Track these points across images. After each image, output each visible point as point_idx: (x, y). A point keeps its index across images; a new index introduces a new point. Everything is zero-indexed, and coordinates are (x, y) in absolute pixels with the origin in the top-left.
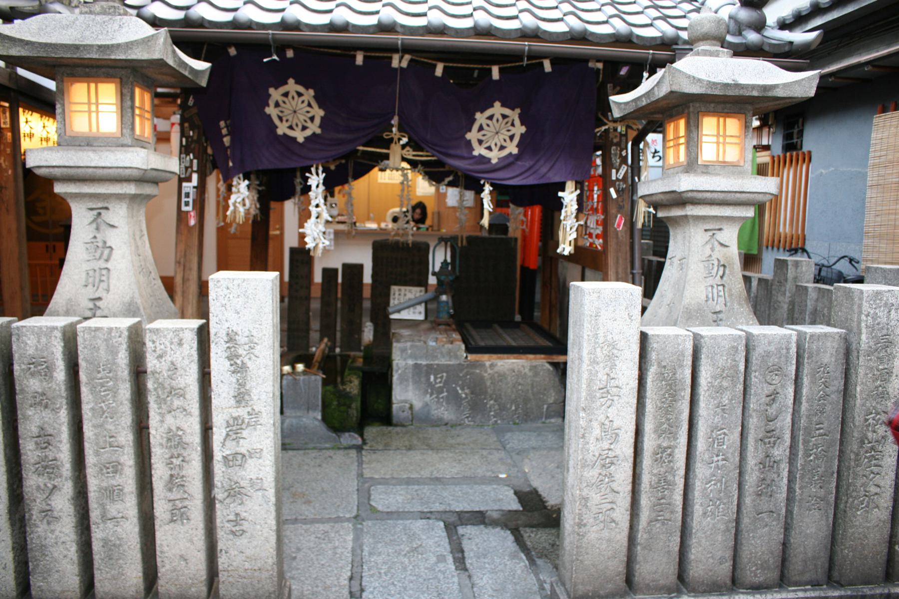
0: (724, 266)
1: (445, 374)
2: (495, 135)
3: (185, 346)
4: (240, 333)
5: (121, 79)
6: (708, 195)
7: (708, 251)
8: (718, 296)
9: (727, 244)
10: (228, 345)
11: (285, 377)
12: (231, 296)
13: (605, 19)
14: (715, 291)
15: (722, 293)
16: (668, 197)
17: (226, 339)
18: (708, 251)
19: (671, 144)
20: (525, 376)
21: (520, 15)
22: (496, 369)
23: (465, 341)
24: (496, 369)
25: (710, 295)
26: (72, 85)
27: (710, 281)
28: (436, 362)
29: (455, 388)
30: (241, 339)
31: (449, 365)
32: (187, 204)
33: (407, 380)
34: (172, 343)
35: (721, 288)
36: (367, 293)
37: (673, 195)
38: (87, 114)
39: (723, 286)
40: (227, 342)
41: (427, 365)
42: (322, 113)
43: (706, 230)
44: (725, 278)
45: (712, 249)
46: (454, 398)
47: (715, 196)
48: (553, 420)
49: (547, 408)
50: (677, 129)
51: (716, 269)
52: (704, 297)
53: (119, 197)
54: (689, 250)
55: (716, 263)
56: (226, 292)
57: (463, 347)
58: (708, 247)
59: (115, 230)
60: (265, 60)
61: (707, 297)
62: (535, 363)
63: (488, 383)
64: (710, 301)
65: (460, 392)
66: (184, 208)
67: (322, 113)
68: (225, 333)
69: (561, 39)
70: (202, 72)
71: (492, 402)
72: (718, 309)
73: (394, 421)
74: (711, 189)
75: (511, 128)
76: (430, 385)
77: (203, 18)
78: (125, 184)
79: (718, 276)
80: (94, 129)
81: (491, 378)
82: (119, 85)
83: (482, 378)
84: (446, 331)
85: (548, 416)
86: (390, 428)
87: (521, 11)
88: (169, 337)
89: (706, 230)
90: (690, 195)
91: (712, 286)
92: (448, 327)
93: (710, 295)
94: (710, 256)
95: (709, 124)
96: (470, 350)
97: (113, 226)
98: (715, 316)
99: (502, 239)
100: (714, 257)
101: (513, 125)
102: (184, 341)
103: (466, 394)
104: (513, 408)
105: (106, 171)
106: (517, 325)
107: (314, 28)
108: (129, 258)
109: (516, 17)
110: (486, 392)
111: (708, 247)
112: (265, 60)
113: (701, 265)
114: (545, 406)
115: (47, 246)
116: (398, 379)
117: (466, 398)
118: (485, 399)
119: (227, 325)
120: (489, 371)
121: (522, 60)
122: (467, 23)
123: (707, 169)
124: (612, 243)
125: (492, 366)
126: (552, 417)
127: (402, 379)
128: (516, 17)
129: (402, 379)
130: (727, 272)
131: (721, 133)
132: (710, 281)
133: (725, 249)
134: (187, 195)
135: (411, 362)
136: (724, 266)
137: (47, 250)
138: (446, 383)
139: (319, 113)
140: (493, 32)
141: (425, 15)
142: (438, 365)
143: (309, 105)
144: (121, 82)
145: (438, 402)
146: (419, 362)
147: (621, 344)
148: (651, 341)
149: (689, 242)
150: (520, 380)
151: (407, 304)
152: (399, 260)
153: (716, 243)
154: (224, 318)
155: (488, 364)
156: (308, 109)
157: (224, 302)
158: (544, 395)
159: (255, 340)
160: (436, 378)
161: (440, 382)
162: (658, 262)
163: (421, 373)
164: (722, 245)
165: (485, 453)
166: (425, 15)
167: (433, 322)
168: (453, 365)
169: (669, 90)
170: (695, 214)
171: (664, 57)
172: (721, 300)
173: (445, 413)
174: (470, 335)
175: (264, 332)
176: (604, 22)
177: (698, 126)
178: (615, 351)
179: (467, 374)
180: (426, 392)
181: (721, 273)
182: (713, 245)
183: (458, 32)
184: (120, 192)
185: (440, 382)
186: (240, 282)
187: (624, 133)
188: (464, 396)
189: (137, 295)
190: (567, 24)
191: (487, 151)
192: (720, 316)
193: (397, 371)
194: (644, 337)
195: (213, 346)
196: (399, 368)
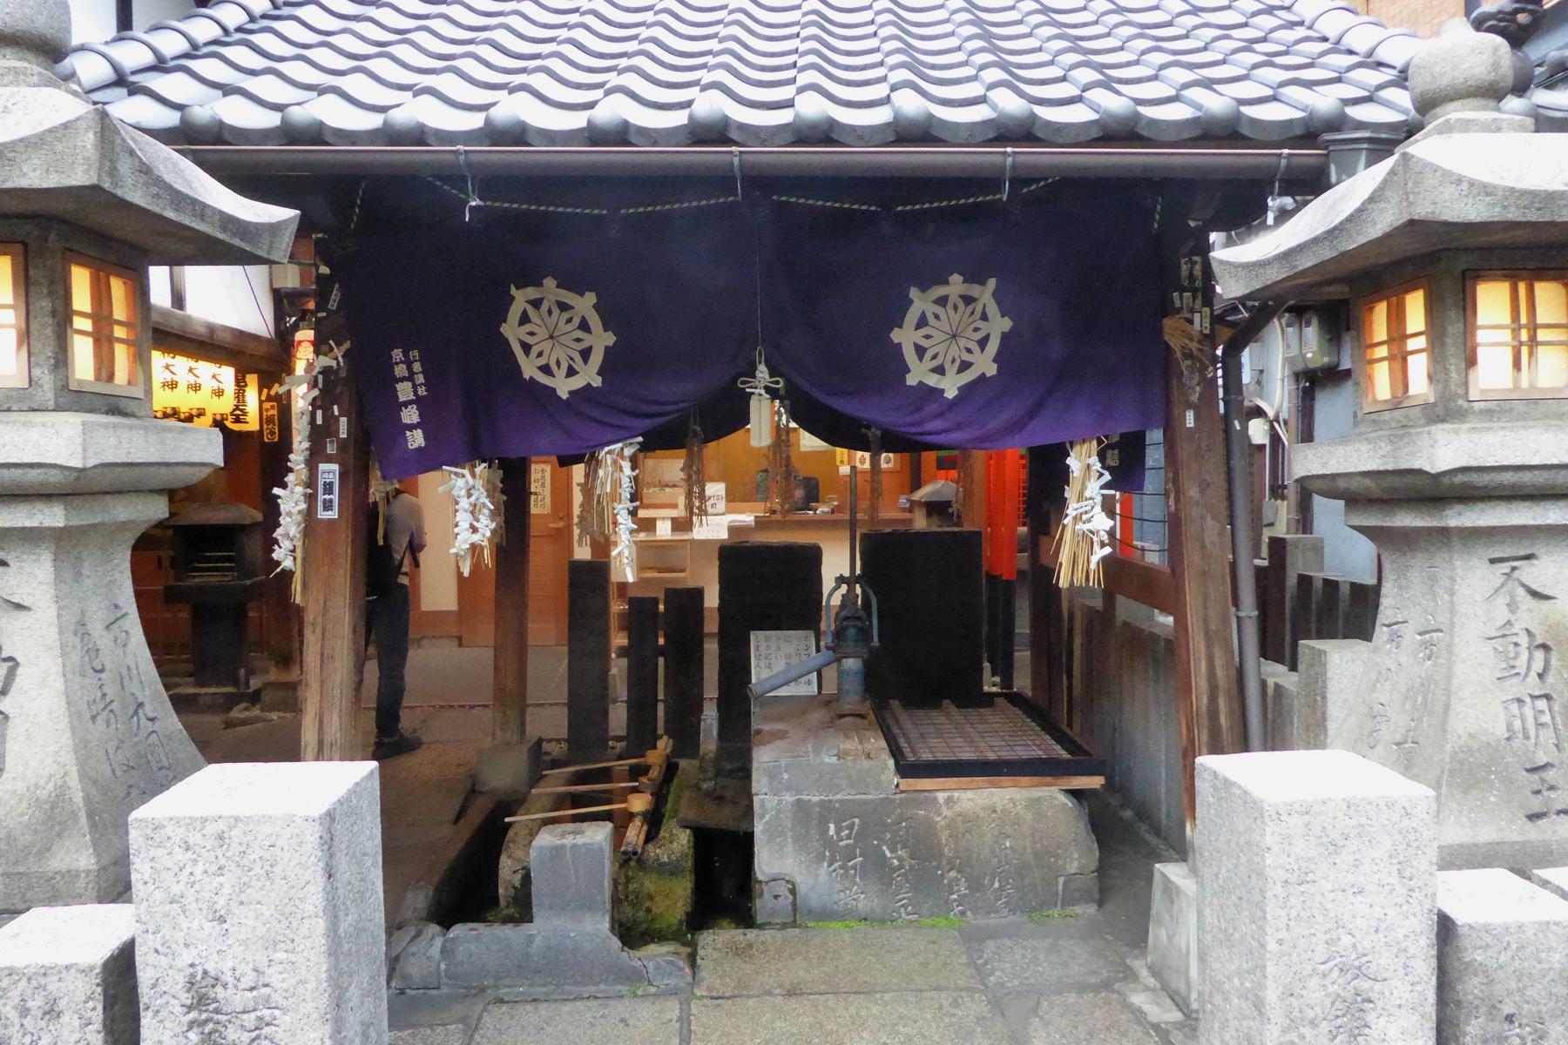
0: (1545, 647)
1: (857, 821)
2: (950, 340)
3: (65, 1018)
4: (228, 978)
5: (25, 244)
6: (1508, 478)
7: (1502, 614)
8: (1539, 725)
9: (1550, 593)
10: (193, 1015)
12: (198, 870)
13: (1173, 93)
14: (1528, 712)
15: (1546, 718)
16: (1387, 482)
17: (186, 998)
18: (1502, 614)
19: (1382, 351)
20: (1017, 822)
21: (991, 94)
22: (957, 808)
23: (896, 752)
24: (957, 808)
25: (1517, 724)
27: (1514, 688)
28: (839, 797)
29: (879, 846)
30: (232, 998)
31: (866, 802)
32: (328, 506)
33: (782, 834)
34: (24, 1012)
35: (1542, 704)
36: (711, 625)
37: (1409, 479)
39: (1548, 697)
40: (190, 1008)
41: (821, 803)
43: (1492, 561)
44: (1550, 679)
45: (1512, 606)
46: (878, 868)
47: (1526, 477)
48: (1078, 909)
49: (1065, 884)
50: (1397, 318)
51: (1525, 656)
52: (1501, 731)
53: (30, 537)
54: (1453, 613)
55: (1524, 640)
56: (180, 856)
57: (891, 763)
58: (1502, 601)
59: (23, 615)
61: (1509, 728)
62: (1037, 793)
63: (944, 837)
64: (1518, 742)
65: (888, 854)
66: (323, 515)
68: (181, 980)
69: (1083, 138)
70: (274, 229)
71: (953, 874)
72: (1542, 759)
73: (759, 920)
74: (1518, 461)
75: (980, 324)
76: (828, 843)
77: (322, 123)
78: (40, 505)
79: (1533, 675)
80: (1522, 287)
81: (948, 826)
82: (21, 259)
83: (930, 827)
84: (856, 729)
85: (1069, 901)
86: (752, 934)
87: (991, 87)
88: (15, 994)
89: (1492, 561)
90: (1459, 479)
91: (1520, 701)
92: (859, 721)
93: (1517, 724)
94: (1509, 622)
95: (1492, 300)
96: (907, 769)
97: (19, 607)
98: (1535, 777)
99: (955, 533)
100: (1518, 627)
101: (984, 317)
102: (62, 1004)
103: (900, 859)
104: (997, 885)
105: (33, 474)
106: (988, 700)
107: (550, 137)
108: (60, 685)
109: (982, 100)
110: (941, 854)
111: (1502, 601)
113: (1488, 648)
114: (1061, 880)
115: (159, 559)
117: (901, 867)
118: (938, 868)
119: (187, 957)
120: (945, 812)
121: (999, 190)
122: (880, 116)
123: (1502, 410)
124: (1193, 558)
125: (949, 800)
126: (1075, 902)
128: (982, 100)
129: (774, 833)
130: (1554, 662)
131: (1524, 320)
132: (1514, 688)
133: (1545, 605)
134: (328, 488)
135: (789, 798)
136: (1545, 647)
137: (160, 565)
138: (860, 837)
140: (935, 133)
141: (789, 104)
142: (842, 802)
144: (26, 253)
145: (846, 875)
147: (1384, 961)
148: (1465, 943)
149: (1452, 593)
150: (1007, 829)
151: (779, 661)
152: (767, 583)
153: (1521, 591)
154: (179, 935)
155: (941, 796)
157: (177, 889)
158: (1056, 856)
159: (277, 998)
160: (839, 830)
161: (849, 837)
163: (809, 819)
164: (1535, 594)
165: (945, 999)
166: (789, 104)
167: (829, 712)
168: (872, 801)
169: (1406, 217)
170: (1468, 524)
171: (1310, 161)
172: (1547, 736)
173: (863, 898)
174: (900, 727)
175: (303, 973)
176: (1170, 98)
177: (1467, 306)
178: (1365, 985)
179: (901, 818)
180: (820, 858)
181: (1538, 665)
182: (1512, 597)
183: (861, 135)
184: (28, 524)
185: (849, 837)
186: (222, 826)
187: (1207, 332)
188: (896, 862)
189: (74, 781)
190: (1093, 107)
191: (936, 377)
192: (1550, 775)
193: (762, 817)
194: (1445, 928)
195: (146, 1020)
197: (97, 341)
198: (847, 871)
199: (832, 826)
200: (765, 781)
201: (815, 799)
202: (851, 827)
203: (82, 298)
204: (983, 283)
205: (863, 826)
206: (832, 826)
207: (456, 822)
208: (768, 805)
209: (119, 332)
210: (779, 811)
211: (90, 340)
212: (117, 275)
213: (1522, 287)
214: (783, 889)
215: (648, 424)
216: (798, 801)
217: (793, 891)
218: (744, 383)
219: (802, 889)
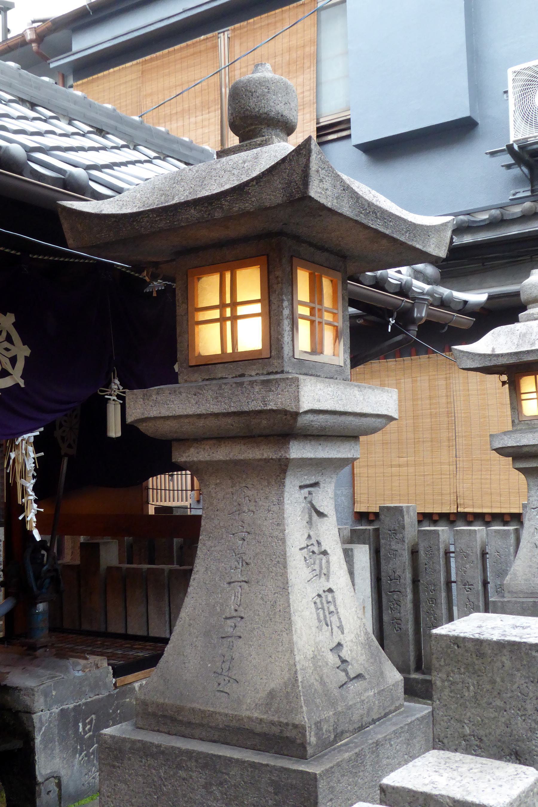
1: (93, 716)
11: (161, 729)
26: (199, 279)
28: (84, 701)
38: (218, 325)
42: (26, 351)
60: (389, 330)
67: (26, 351)
76: (80, 739)
80: (229, 350)
105: (330, 420)
112: (389, 330)
116: (43, 740)
127: (47, 741)
135: (56, 710)
139: (23, 352)
142: (86, 704)
143: (9, 339)
146: (65, 707)
156: (7, 345)
161: (90, 730)
162: (132, 563)
168: (102, 699)
196: (42, 724)
197: (312, 322)
198: (89, 757)
199: (80, 725)
200: (42, 700)
201: (71, 706)
202: (90, 723)
203: (303, 291)
204: (390, 322)
205: (97, 719)
206: (80, 725)
207: (340, 688)
208: (44, 719)
209: (327, 317)
210: (50, 722)
211: (308, 323)
212: (327, 275)
213: (229, 350)
214: (52, 785)
215: (50, 418)
216: (62, 710)
217: (59, 785)
218: (102, 391)
219: (65, 780)
